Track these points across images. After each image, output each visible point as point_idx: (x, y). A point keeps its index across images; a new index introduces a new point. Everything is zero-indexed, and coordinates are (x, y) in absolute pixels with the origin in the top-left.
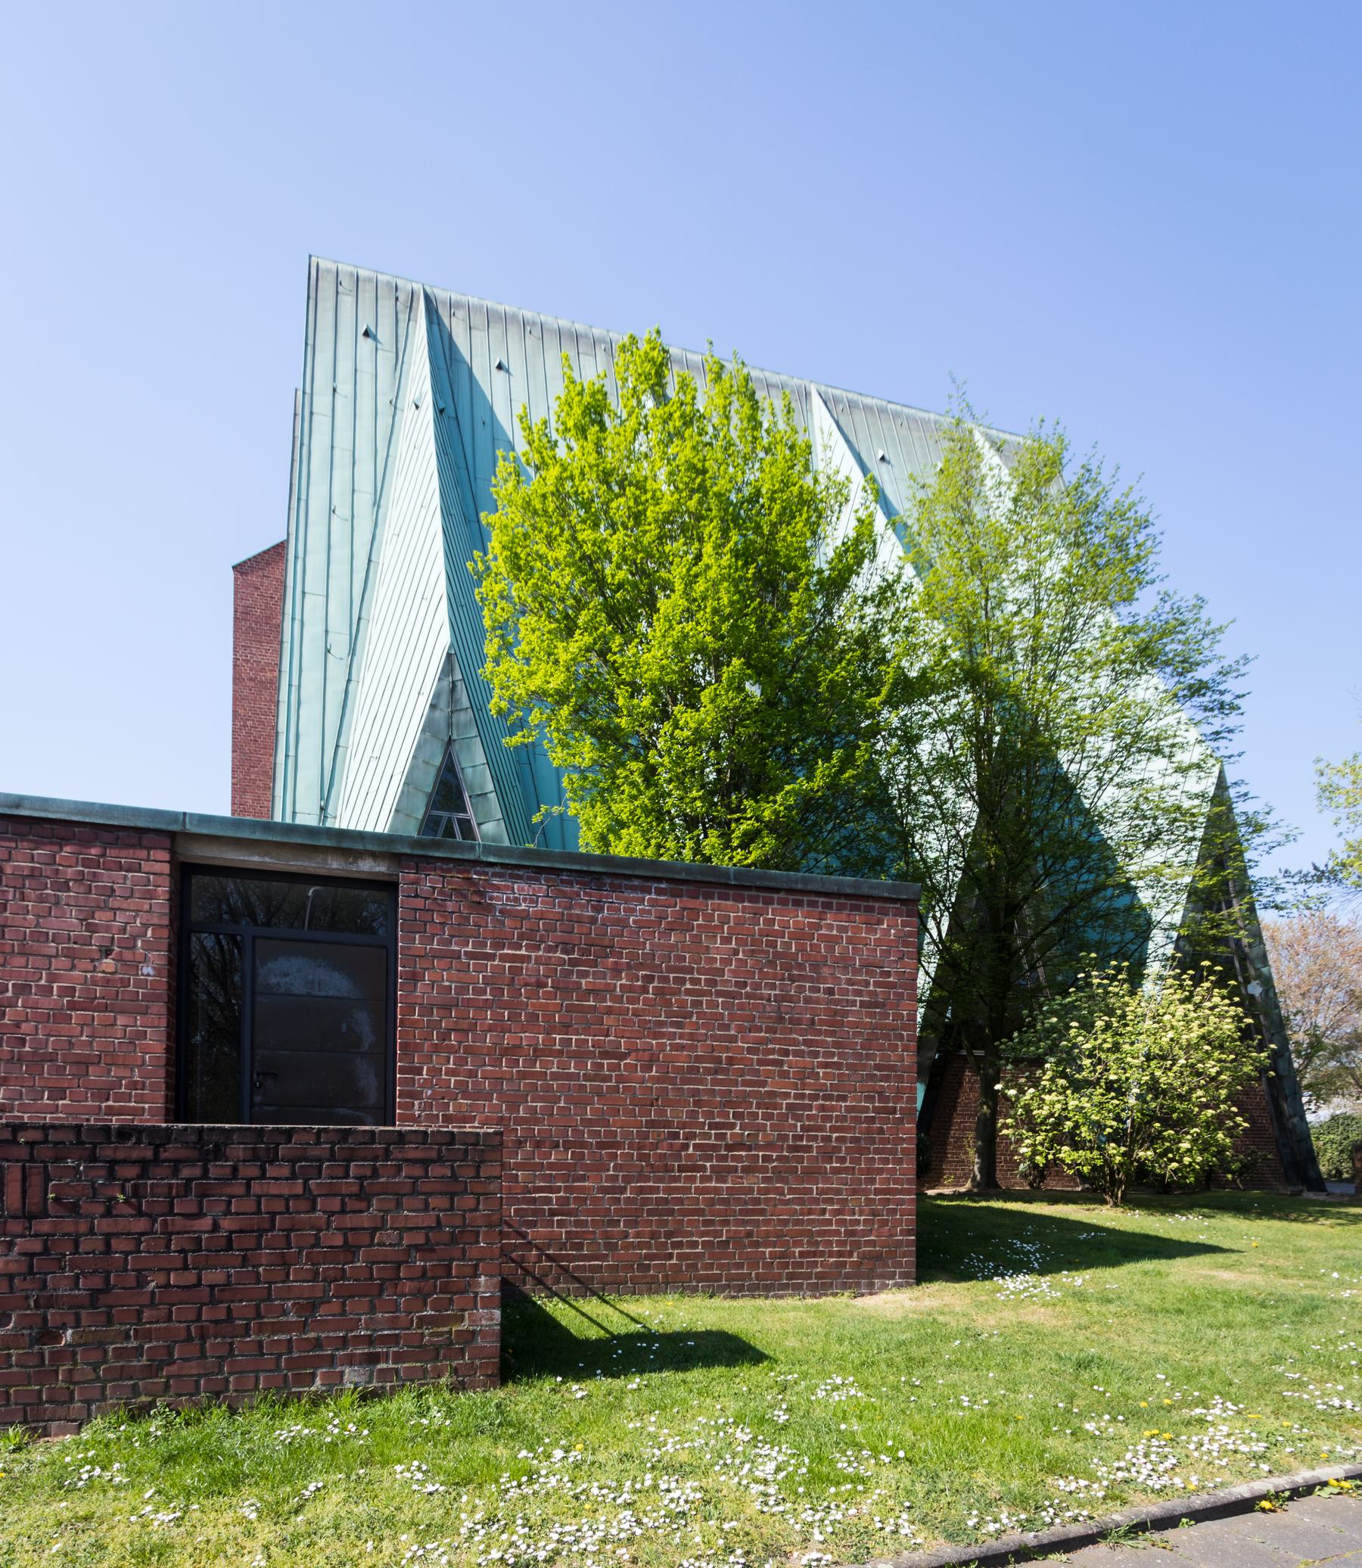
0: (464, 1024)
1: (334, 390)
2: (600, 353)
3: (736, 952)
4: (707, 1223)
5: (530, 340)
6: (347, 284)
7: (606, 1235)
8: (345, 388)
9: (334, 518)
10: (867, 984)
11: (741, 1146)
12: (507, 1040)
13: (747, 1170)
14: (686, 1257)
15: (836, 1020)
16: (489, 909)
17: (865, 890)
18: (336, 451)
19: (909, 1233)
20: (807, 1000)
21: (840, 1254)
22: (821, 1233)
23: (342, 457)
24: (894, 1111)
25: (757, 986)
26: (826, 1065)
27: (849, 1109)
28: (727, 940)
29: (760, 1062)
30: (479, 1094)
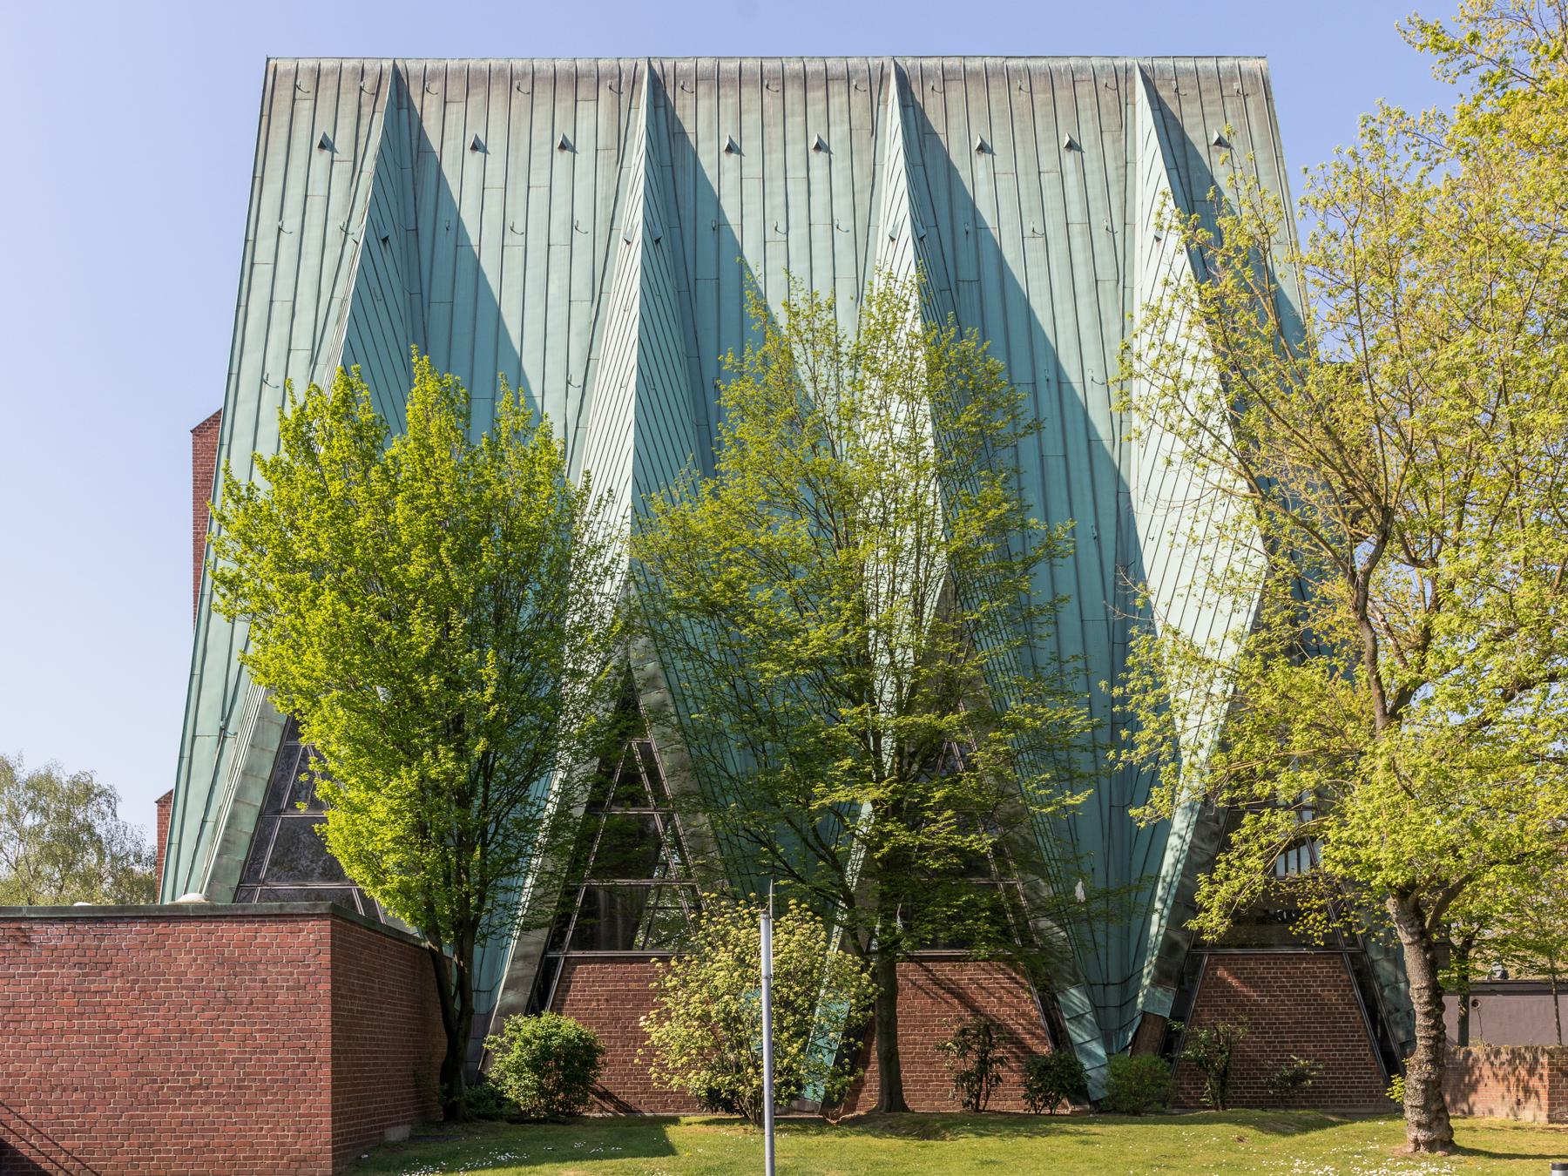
0: (18, 1017)
1: (280, 229)
2: (604, 93)
3: (195, 960)
4: (177, 1137)
5: (519, 100)
6: (305, 82)
7: (109, 1146)
8: (292, 223)
9: (266, 388)
10: (292, 974)
11: (200, 1086)
12: (45, 1025)
13: (205, 1103)
14: (163, 1159)
15: (270, 999)
16: (30, 945)
17: (287, 910)
18: (276, 305)
19: (326, 1143)
20: (247, 988)
21: (273, 1158)
22: (259, 1144)
23: (281, 311)
24: (314, 1060)
25: (210, 982)
26: (261, 1031)
27: (280, 1060)
28: (190, 952)
29: (213, 1031)
30: (28, 1060)
